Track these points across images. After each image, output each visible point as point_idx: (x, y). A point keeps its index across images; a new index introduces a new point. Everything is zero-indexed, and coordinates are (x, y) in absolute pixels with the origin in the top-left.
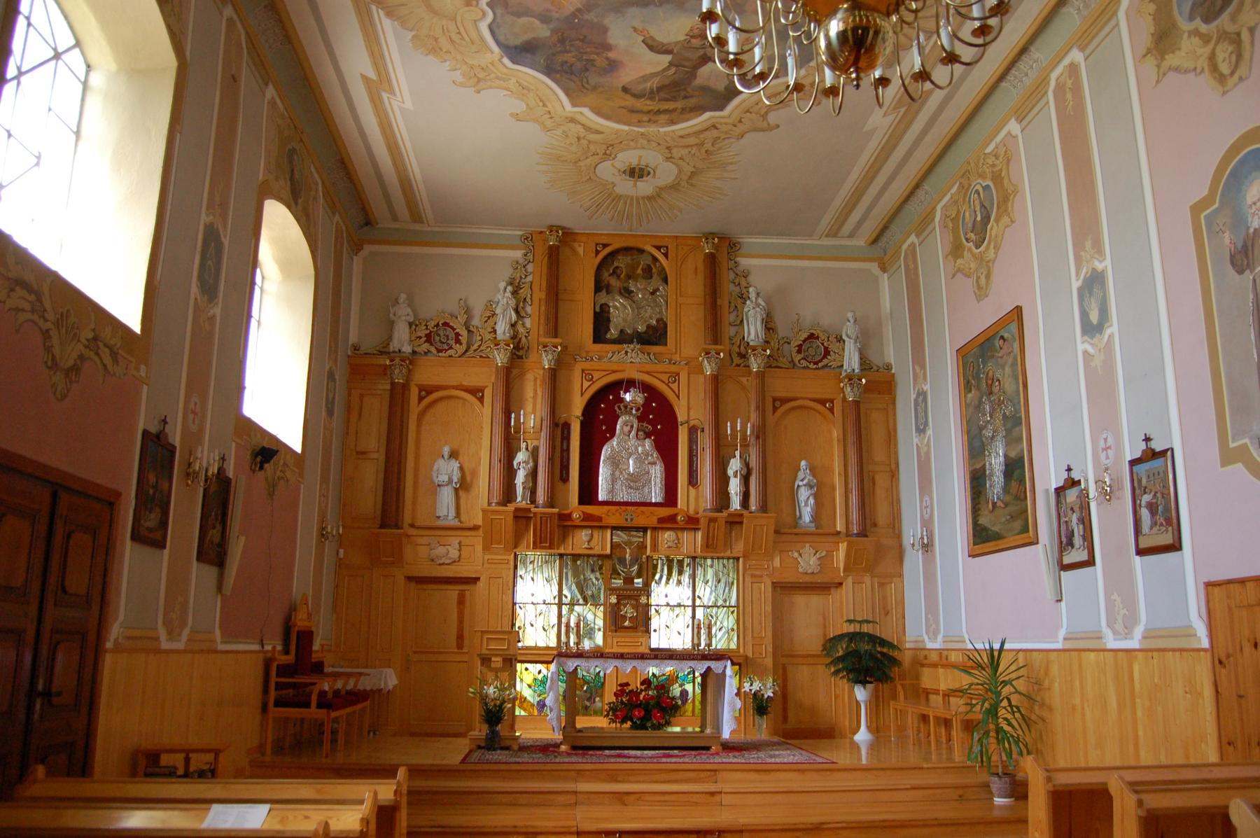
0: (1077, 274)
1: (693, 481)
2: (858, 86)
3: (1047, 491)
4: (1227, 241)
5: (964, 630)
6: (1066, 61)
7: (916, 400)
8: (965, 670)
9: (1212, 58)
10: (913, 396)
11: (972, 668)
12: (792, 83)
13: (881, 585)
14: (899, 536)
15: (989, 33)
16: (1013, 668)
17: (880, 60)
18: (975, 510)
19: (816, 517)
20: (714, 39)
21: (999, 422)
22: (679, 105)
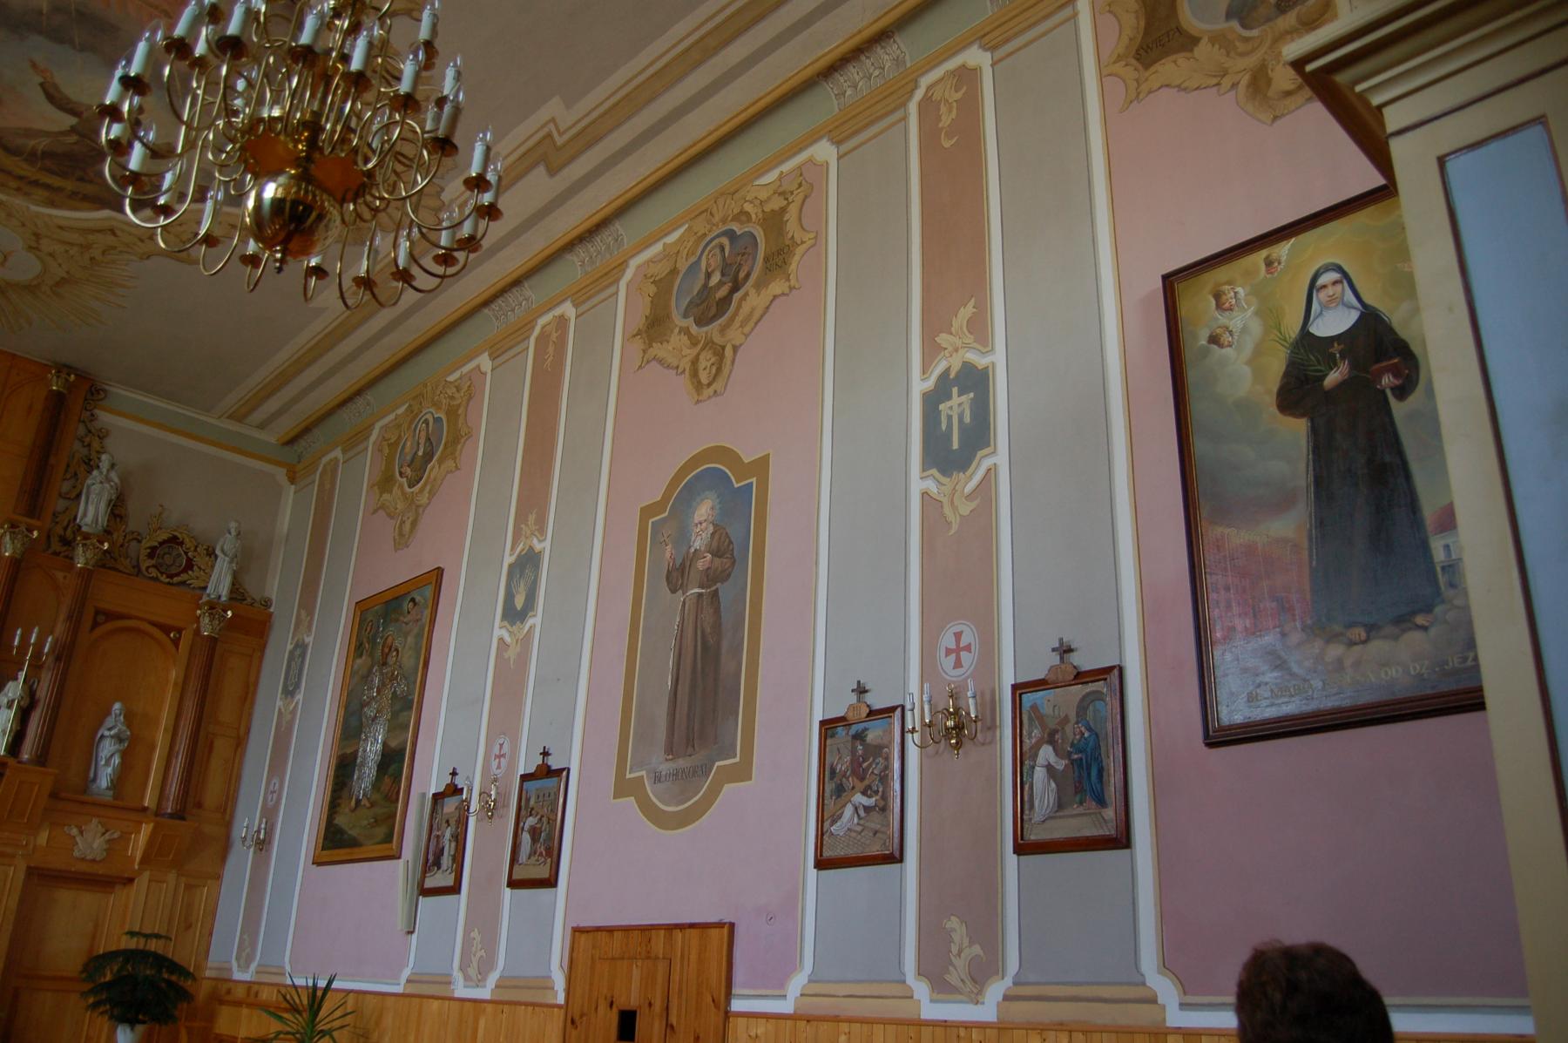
0: (513, 549)
1: (753, 309)
2: (280, 270)
3: (424, 795)
4: (668, 555)
5: (287, 959)
6: (558, 312)
7: (292, 652)
8: (272, 1011)
9: (695, 362)
10: (289, 647)
11: (286, 1010)
12: (202, 232)
13: (189, 887)
14: (228, 825)
15: (453, 265)
16: (338, 1013)
17: (318, 248)
18: (334, 806)
19: (118, 783)
20: (110, 142)
21: (386, 701)
22: (69, 185)
